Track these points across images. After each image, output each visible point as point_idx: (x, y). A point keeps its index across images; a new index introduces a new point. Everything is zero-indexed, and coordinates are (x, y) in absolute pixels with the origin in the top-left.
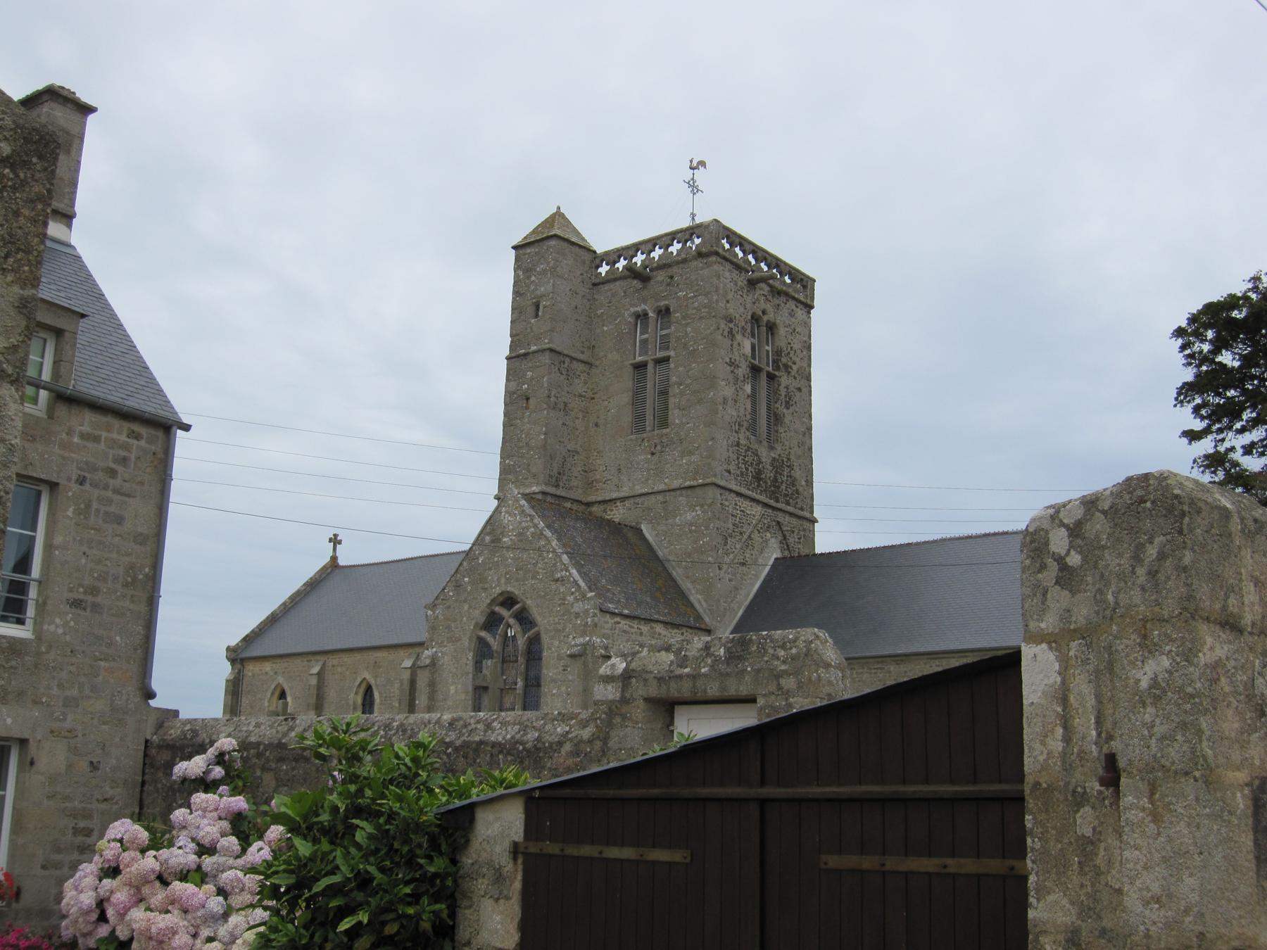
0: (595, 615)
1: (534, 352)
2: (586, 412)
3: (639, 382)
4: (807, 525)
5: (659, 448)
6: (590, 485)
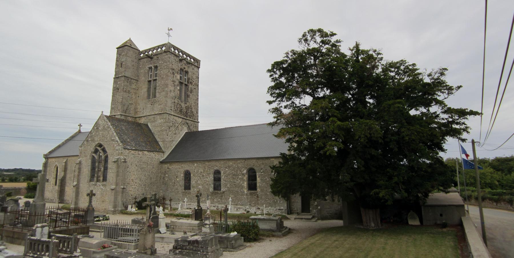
0: (122, 150)
1: (120, 77)
2: (136, 93)
3: (150, 85)
4: (196, 123)
5: (153, 103)
6: (136, 113)
